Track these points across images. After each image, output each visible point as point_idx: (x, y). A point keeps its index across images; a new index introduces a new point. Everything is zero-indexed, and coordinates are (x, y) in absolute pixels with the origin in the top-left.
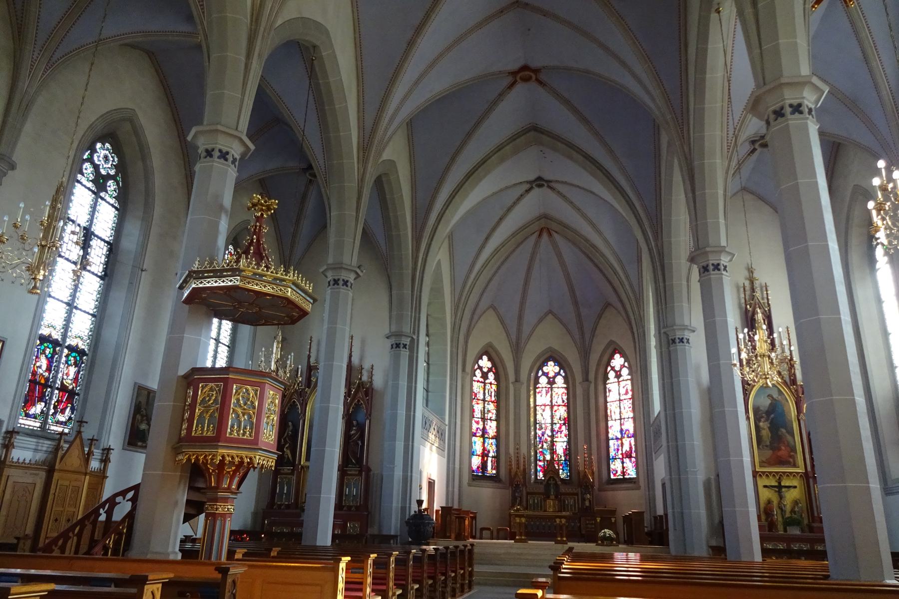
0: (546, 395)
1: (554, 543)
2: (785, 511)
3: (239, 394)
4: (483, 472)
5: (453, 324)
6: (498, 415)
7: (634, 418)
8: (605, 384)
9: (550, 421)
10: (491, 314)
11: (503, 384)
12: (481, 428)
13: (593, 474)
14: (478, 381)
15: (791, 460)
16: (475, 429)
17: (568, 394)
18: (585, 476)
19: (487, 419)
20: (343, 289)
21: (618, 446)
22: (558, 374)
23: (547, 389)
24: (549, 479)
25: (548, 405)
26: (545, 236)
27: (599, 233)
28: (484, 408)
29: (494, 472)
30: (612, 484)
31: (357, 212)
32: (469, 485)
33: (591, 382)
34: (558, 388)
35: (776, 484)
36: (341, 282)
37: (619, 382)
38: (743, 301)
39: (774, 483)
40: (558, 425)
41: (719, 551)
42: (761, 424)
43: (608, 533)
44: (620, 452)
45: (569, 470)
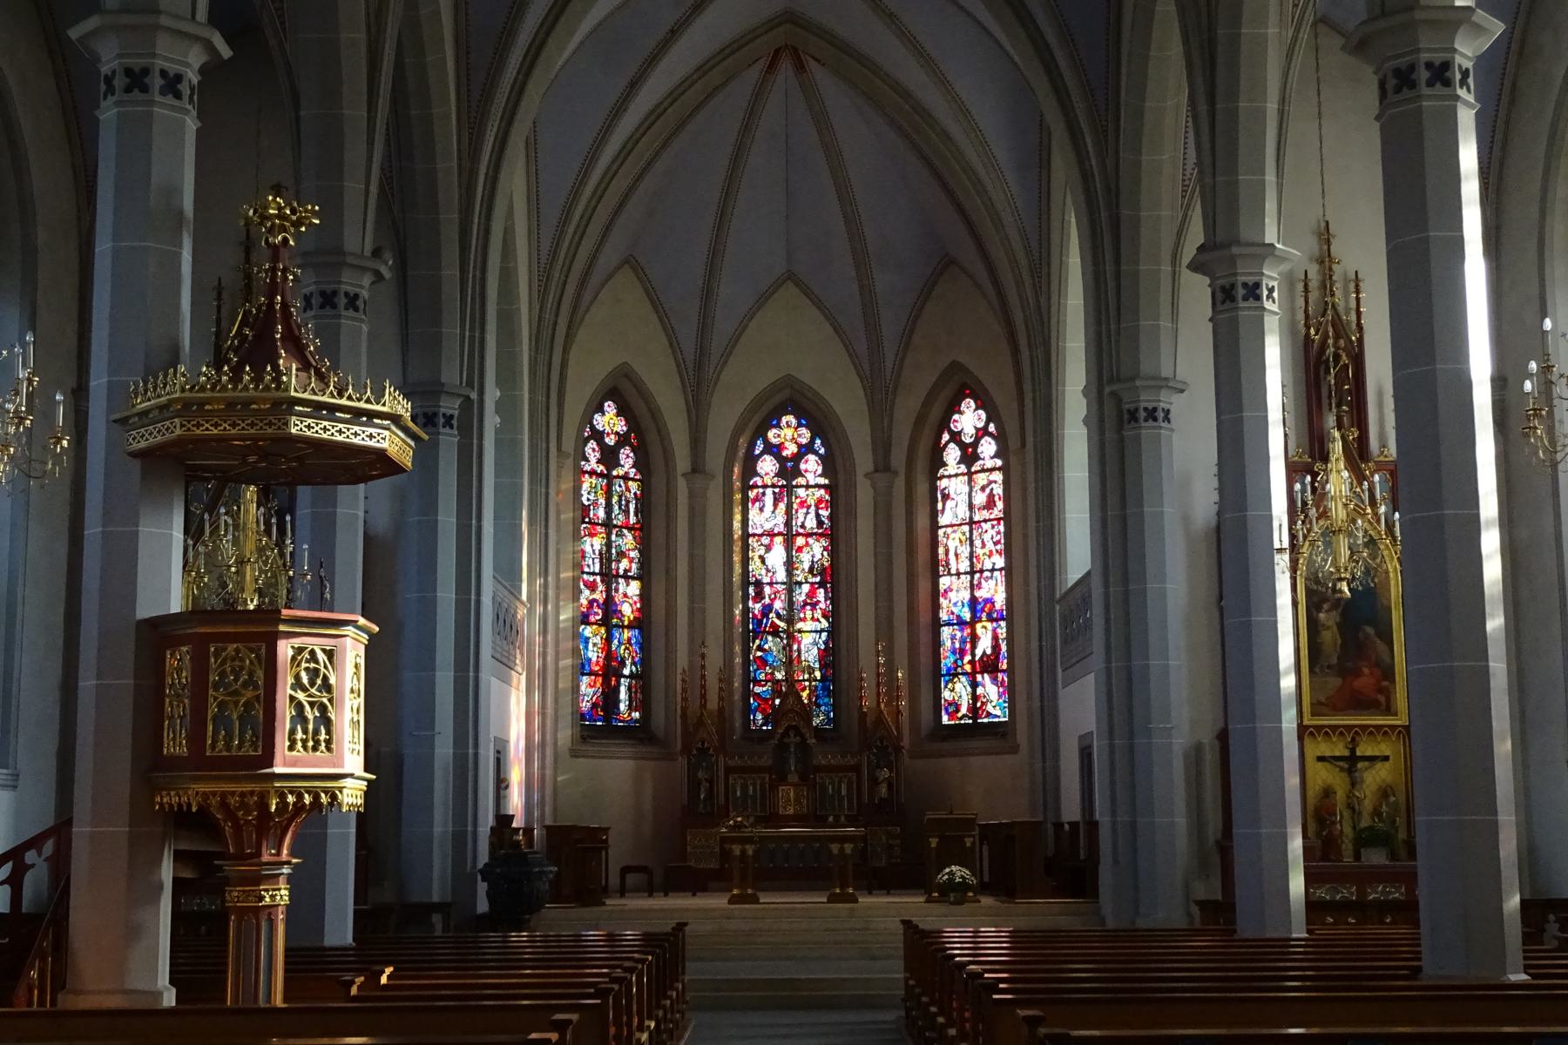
1: (922, 899)
2: (1360, 813)
3: (298, 665)
4: (607, 718)
5: (535, 325)
6: (644, 563)
7: (1008, 570)
8: (934, 478)
9: (781, 575)
10: (626, 278)
11: (658, 482)
12: (601, 601)
14: (592, 473)
15: (1382, 699)
17: (833, 505)
19: (617, 576)
20: (348, 318)
21: (963, 641)
23: (777, 490)
24: (786, 734)
25: (780, 534)
26: (786, 68)
27: (943, 83)
29: (636, 715)
30: (944, 739)
31: (369, 112)
32: (574, 754)
33: (896, 473)
34: (808, 487)
35: (1346, 753)
36: (342, 301)
37: (970, 474)
38: (1301, 316)
39: (1340, 750)
40: (806, 588)
41: (1220, 912)
42: (1322, 616)
44: (968, 658)
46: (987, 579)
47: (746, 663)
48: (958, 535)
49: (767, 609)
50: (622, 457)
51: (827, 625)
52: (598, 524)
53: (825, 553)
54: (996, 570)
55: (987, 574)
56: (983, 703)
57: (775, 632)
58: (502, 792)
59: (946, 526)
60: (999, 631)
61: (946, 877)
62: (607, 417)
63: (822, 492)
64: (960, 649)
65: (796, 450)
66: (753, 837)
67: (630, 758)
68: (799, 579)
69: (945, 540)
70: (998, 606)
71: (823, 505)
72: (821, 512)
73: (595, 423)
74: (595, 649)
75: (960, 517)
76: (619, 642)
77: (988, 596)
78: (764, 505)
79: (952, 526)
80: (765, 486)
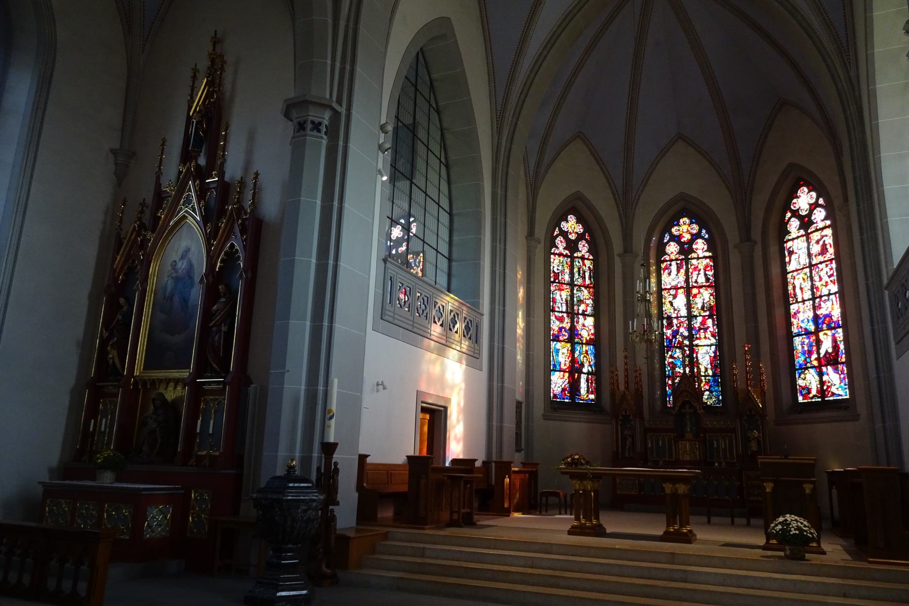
0: (678, 271)
5: (495, 148)
6: (596, 307)
7: (841, 293)
9: (684, 312)
12: (568, 328)
13: (763, 394)
14: (560, 255)
16: (557, 329)
17: (716, 268)
18: (749, 398)
19: (578, 314)
21: (810, 345)
22: (698, 236)
23: (679, 262)
24: (684, 404)
25: (682, 287)
28: (572, 296)
29: (592, 397)
32: (546, 417)
33: (755, 243)
34: (698, 258)
37: (807, 235)
40: (700, 319)
43: (794, 524)
44: (814, 356)
45: (721, 391)
46: (825, 301)
47: (663, 366)
48: (802, 275)
49: (675, 334)
50: (580, 246)
51: (715, 341)
52: (565, 284)
53: (712, 297)
54: (832, 294)
55: (823, 298)
56: (828, 387)
57: (681, 346)
58: (327, 422)
59: (793, 271)
60: (837, 335)
61: (780, 527)
62: (570, 224)
63: (708, 260)
64: (808, 350)
65: (690, 238)
66: (586, 474)
67: (585, 422)
68: (695, 314)
69: (792, 281)
70: (835, 319)
71: (709, 269)
72: (707, 272)
73: (562, 226)
74: (564, 356)
75: (802, 264)
76: (580, 352)
77: (827, 312)
78: (671, 272)
79: (797, 270)
80: (671, 260)
